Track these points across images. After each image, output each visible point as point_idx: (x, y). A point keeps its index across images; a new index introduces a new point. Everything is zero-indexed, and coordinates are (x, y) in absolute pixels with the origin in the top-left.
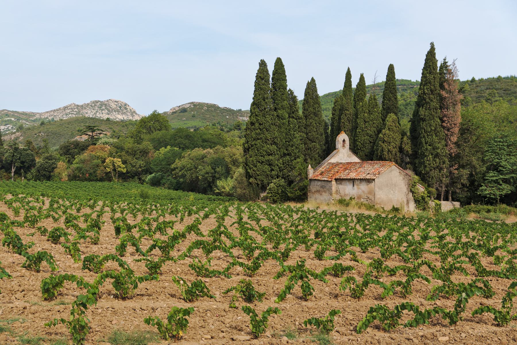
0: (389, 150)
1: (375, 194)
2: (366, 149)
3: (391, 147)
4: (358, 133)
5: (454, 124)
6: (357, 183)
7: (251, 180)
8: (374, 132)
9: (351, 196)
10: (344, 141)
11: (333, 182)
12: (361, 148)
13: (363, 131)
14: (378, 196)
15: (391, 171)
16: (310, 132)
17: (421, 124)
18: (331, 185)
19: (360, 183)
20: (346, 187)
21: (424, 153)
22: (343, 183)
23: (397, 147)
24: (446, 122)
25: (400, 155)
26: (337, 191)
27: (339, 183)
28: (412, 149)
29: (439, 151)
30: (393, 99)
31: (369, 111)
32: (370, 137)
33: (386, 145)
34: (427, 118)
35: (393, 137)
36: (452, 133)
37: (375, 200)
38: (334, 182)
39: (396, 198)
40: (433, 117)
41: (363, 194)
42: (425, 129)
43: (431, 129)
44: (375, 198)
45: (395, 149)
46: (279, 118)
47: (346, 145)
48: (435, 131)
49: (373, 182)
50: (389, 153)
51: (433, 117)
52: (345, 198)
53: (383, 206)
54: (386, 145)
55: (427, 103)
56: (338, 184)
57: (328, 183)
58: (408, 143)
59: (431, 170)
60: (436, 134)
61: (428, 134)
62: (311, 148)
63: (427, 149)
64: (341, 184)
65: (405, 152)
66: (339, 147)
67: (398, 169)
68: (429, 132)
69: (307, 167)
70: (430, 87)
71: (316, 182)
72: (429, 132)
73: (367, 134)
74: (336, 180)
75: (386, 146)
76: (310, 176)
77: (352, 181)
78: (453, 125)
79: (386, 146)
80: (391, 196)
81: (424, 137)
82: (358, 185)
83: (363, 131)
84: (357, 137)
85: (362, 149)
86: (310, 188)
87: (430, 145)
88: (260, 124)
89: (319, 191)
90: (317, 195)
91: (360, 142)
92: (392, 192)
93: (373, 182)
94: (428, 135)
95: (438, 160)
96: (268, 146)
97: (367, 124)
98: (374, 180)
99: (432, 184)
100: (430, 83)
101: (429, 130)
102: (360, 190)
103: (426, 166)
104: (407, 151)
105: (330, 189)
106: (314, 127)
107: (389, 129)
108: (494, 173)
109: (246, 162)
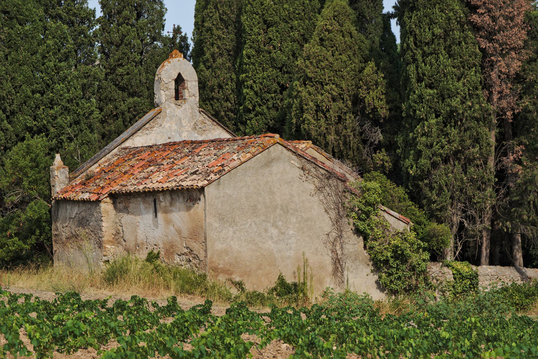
0: (318, 106)
1: (205, 239)
2: (268, 108)
3: (323, 98)
4: (246, 60)
5: (507, 18)
6: (163, 204)
10: (179, 80)
11: (102, 205)
12: (254, 106)
13: (258, 51)
14: (219, 246)
15: (269, 163)
16: (121, 65)
19: (171, 204)
20: (138, 218)
21: (415, 111)
23: (346, 97)
24: (480, 11)
27: (120, 206)
28: (388, 102)
29: (455, 102)
32: (281, 69)
33: (311, 89)
35: (331, 65)
36: (501, 45)
38: (107, 206)
39: (292, 253)
41: (177, 238)
43: (433, 35)
44: (206, 251)
45: (340, 104)
46: (11, 19)
47: (186, 94)
48: (445, 41)
53: (238, 279)
54: (311, 89)
58: (377, 84)
59: (435, 165)
60: (448, 49)
61: (424, 52)
62: (123, 114)
63: (421, 97)
64: (126, 210)
65: (368, 110)
67: (294, 157)
68: (427, 44)
72: (427, 44)
74: (114, 197)
77: (151, 200)
78: (502, 21)
80: (270, 245)
81: (415, 60)
82: (166, 212)
84: (244, 71)
85: (257, 108)
86: (57, 229)
87: (430, 86)
91: (252, 88)
92: (274, 231)
94: (425, 55)
95: (454, 132)
97: (272, 32)
98: (202, 190)
99: (440, 210)
101: (429, 36)
102: (172, 228)
103: (419, 154)
104: (374, 109)
107: (321, 40)
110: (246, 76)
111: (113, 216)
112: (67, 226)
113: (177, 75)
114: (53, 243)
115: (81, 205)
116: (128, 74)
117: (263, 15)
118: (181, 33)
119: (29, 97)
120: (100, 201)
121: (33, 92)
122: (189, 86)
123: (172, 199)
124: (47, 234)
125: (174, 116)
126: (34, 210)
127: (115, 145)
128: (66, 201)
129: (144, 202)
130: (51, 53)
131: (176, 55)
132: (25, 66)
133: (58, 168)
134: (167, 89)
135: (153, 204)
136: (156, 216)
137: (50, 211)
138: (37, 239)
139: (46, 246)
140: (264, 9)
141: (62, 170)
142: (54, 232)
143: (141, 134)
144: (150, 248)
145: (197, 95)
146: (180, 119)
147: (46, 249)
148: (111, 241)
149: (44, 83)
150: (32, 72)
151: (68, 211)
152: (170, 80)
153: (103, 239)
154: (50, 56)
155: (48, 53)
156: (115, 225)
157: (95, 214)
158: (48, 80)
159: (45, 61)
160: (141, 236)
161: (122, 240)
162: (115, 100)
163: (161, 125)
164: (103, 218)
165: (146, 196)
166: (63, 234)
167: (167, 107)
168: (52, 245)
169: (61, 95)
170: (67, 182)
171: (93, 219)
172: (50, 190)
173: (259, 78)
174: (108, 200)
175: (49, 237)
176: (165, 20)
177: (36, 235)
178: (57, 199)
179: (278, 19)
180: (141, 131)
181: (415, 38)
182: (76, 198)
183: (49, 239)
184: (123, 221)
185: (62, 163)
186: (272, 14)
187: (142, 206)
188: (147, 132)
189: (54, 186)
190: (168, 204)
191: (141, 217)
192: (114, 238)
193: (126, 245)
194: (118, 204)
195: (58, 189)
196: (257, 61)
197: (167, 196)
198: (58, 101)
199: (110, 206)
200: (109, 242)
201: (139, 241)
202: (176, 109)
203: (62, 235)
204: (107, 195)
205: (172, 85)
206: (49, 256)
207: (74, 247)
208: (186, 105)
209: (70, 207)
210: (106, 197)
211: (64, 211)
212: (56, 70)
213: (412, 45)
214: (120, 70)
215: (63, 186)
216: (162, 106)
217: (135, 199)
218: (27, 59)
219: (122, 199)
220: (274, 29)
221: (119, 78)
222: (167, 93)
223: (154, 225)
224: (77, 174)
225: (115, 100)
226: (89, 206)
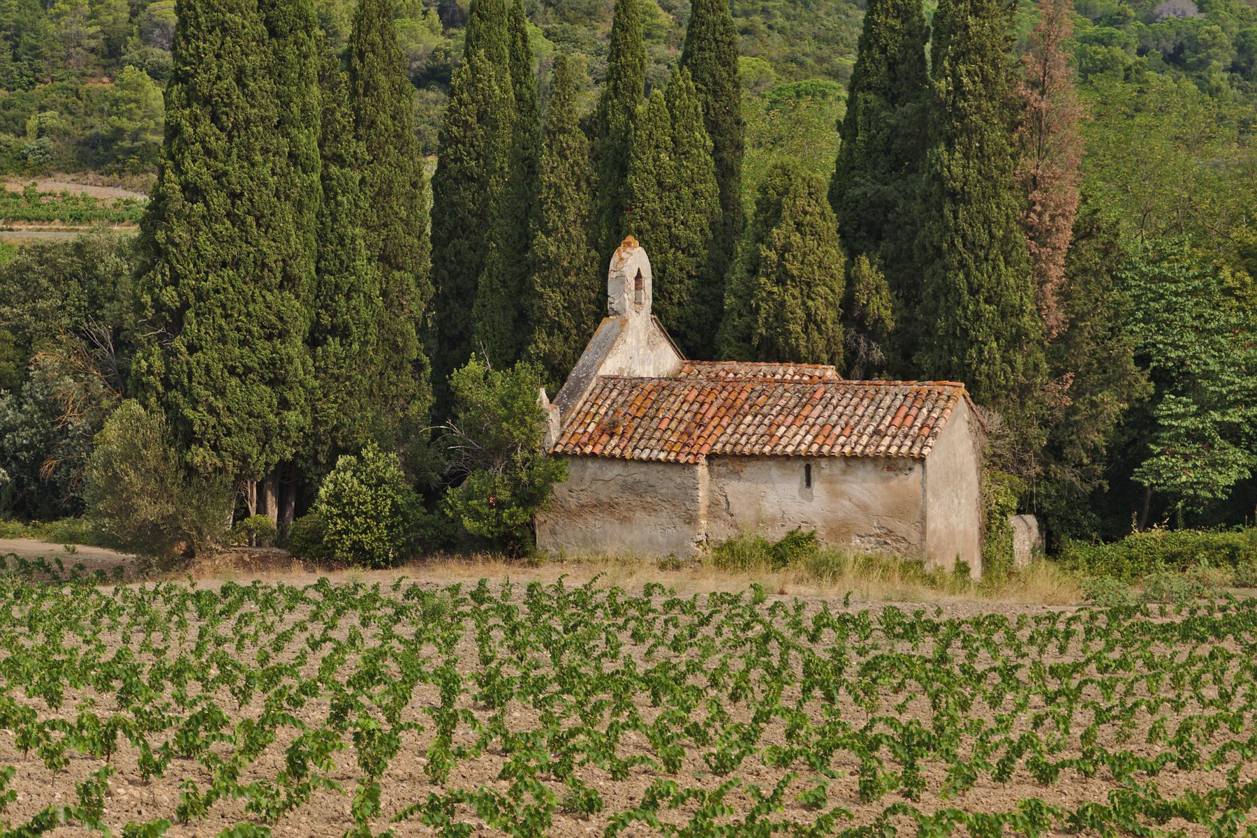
0: (809, 315)
6: (826, 471)
7: (200, 456)
9: (791, 527)
10: (639, 277)
17: (946, 211)
18: (690, 482)
19: (844, 472)
20: (762, 487)
22: (750, 469)
25: (845, 333)
27: (723, 470)
28: (893, 312)
34: (976, 192)
40: (994, 187)
42: (964, 237)
50: (811, 326)
51: (994, 187)
52: (760, 534)
55: (969, 131)
56: (719, 476)
57: (672, 473)
61: (977, 256)
63: (978, 315)
64: (736, 474)
65: (869, 321)
70: (981, 69)
71: (592, 467)
75: (794, 297)
76: (554, 435)
77: (800, 467)
79: (794, 297)
81: (963, 265)
82: (830, 481)
87: (987, 301)
88: (234, 196)
90: (598, 525)
93: (918, 468)
96: (269, 297)
100: (980, 50)
104: (879, 320)
105: (689, 493)
108: (1186, 405)
109: (169, 370)
135: (803, 470)
136: (809, 484)
181: (964, 237)
184: (727, 489)
213: (960, 246)
220: (673, 195)
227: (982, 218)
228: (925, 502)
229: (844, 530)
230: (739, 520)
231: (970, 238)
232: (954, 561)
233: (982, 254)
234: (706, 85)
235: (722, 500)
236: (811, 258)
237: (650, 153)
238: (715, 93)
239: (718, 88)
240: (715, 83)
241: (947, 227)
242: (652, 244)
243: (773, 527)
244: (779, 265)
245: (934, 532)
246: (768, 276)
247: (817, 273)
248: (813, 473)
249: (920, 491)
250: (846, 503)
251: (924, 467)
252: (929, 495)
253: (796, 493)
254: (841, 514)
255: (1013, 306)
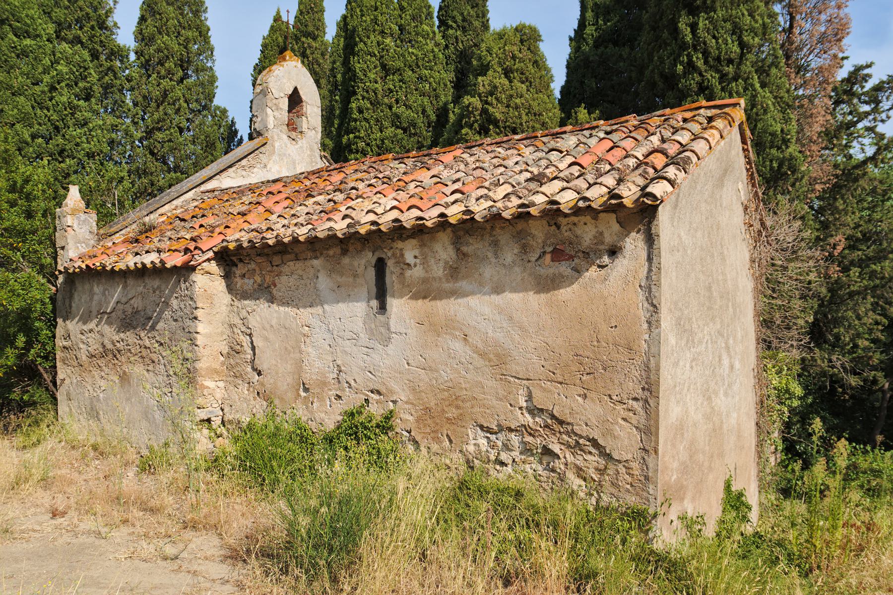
8: (424, 111)
10: (295, 100)
11: (198, 278)
13: (375, 104)
17: (682, 25)
19: (454, 272)
20: (306, 314)
26: (235, 350)
27: (248, 284)
30: (477, 24)
31: (401, 28)
32: (405, 130)
37: (649, 450)
42: (706, 54)
47: (304, 124)
49: (634, 244)
52: (301, 413)
56: (244, 295)
66: (271, 122)
68: (730, 61)
69: (59, 200)
73: (396, 120)
77: (364, 262)
83: (375, 104)
86: (67, 337)
89: (115, 354)
97: (393, 81)
106: (178, 111)
110: (355, 137)
111: (224, 308)
112: (91, 331)
113: (292, 89)
114: (58, 364)
115: (131, 282)
116: (170, 141)
117: (382, 57)
118: (227, 117)
119: (27, 143)
120: (193, 269)
121: (34, 137)
122: (308, 113)
123: (462, 256)
124: (44, 345)
125: (285, 155)
126: (13, 291)
127: (190, 185)
128: (92, 274)
129: (331, 272)
130: (63, 84)
131: (291, 57)
132: (22, 97)
133: (74, 212)
134: (278, 108)
135: (371, 273)
136: (383, 308)
137: (53, 299)
138: (20, 357)
139: (42, 370)
140: (383, 49)
141: (83, 216)
142: (60, 342)
143: (233, 175)
144: (352, 400)
145: (320, 129)
146: (294, 163)
147: (41, 375)
148: (216, 371)
149: (52, 124)
150: (33, 108)
151: (96, 298)
152: (282, 95)
153: (198, 365)
154: (62, 88)
155: (59, 83)
156: (228, 332)
157: (174, 303)
158: (58, 121)
159: (54, 94)
160: (318, 364)
161: (249, 369)
162: (152, 174)
163: (265, 166)
164: (199, 313)
165: (345, 252)
166: (81, 346)
167: (276, 137)
168: (55, 367)
169: (77, 145)
170: (92, 242)
171: (167, 314)
172: (55, 257)
173: (376, 140)
174: (213, 266)
175: (50, 352)
176: (217, 87)
177: (16, 348)
178: (71, 271)
179: (403, 65)
180: (234, 168)
181: (706, 54)
182: (121, 266)
183: (49, 357)
184: (253, 322)
185: (82, 205)
186: (395, 57)
187: (324, 282)
188: (244, 173)
189: (63, 248)
190: (438, 271)
191: (318, 310)
192: (223, 364)
193: (262, 384)
194: (238, 279)
195: (72, 253)
196: (372, 116)
197: (438, 247)
198: (72, 152)
199: (217, 283)
200: (213, 373)
201: (310, 375)
202: (289, 145)
203: (80, 349)
204: (210, 254)
205: (285, 104)
206: (47, 389)
207: (111, 377)
208: (304, 141)
209: (101, 288)
210: (209, 260)
211: (85, 297)
212: (71, 109)
213: (700, 64)
214: (159, 136)
215: (83, 249)
216: (268, 134)
217: (299, 264)
218: (25, 87)
219: (253, 266)
220: (397, 77)
221: (159, 146)
222: (276, 113)
223: (371, 334)
224: (113, 230)
225: (152, 174)
226: (156, 283)
227: (728, 25)
228: (655, 342)
229: (452, 413)
230: (268, 380)
231: (714, 53)
232: (721, 494)
233: (730, 69)
234: (455, 22)
235: (245, 340)
236: (518, 101)
237: (374, 38)
238: (464, 30)
239: (466, 24)
240: (464, 20)
241: (684, 46)
242: (372, 122)
243: (321, 400)
244: (484, 111)
245: (680, 428)
246: (471, 127)
247: (524, 118)
248: (391, 279)
249: (642, 312)
250: (457, 346)
251: (650, 240)
252: (666, 321)
253: (358, 325)
254: (446, 374)
255: (773, 134)
